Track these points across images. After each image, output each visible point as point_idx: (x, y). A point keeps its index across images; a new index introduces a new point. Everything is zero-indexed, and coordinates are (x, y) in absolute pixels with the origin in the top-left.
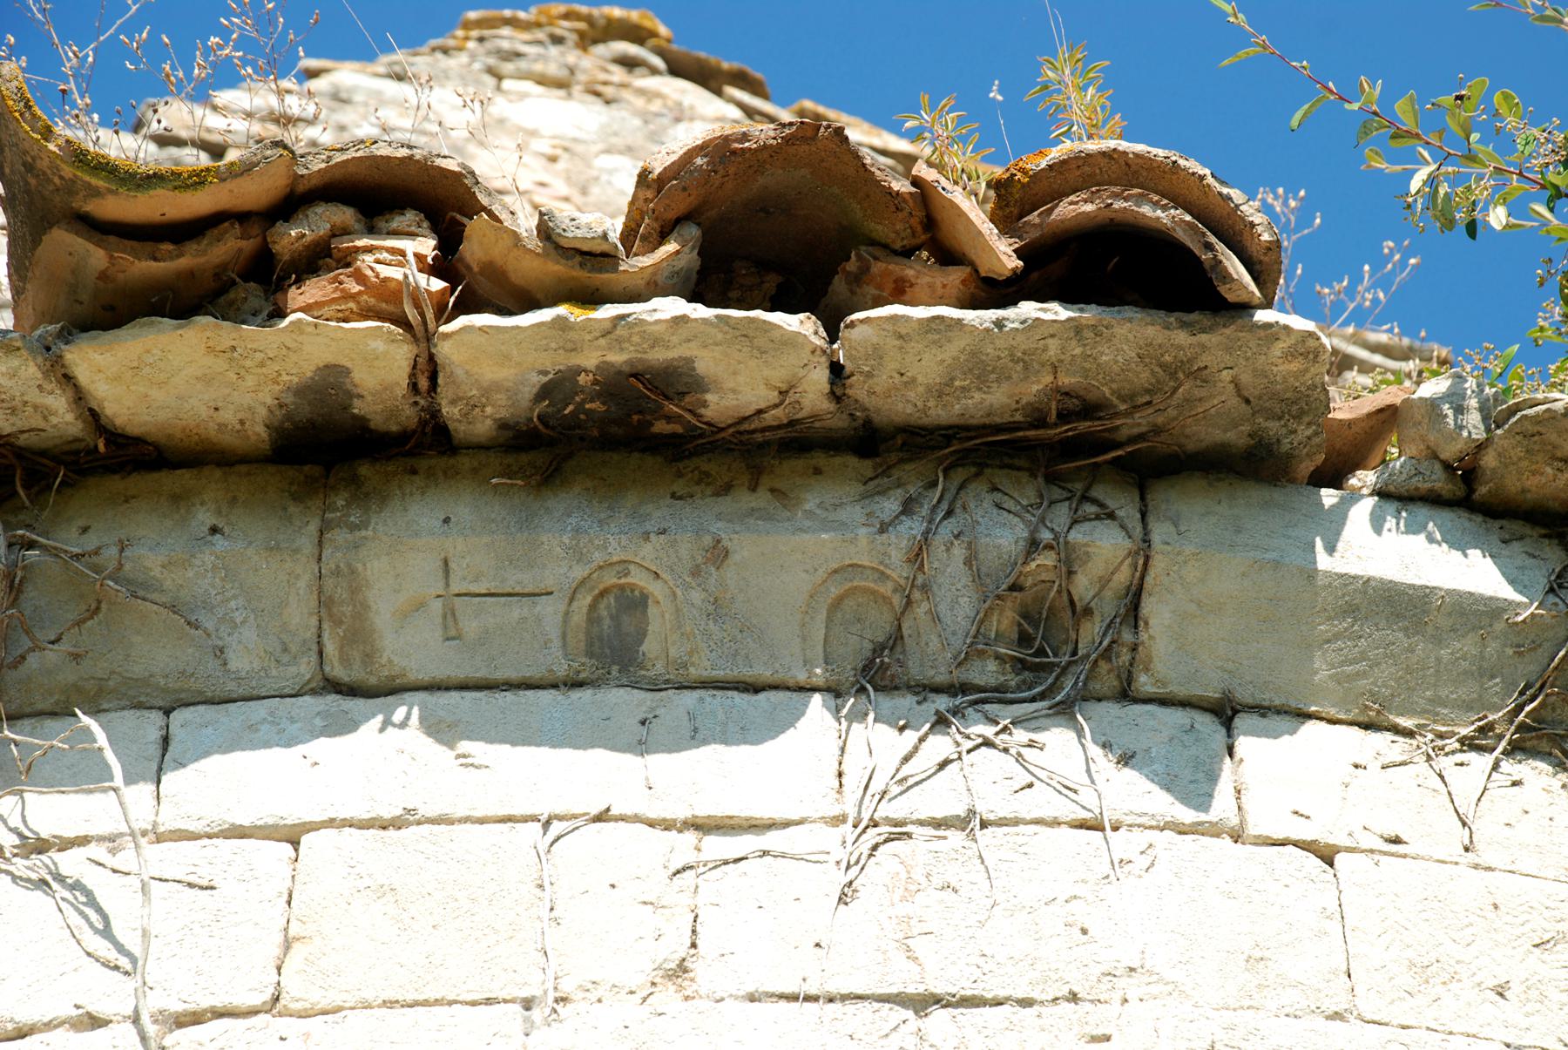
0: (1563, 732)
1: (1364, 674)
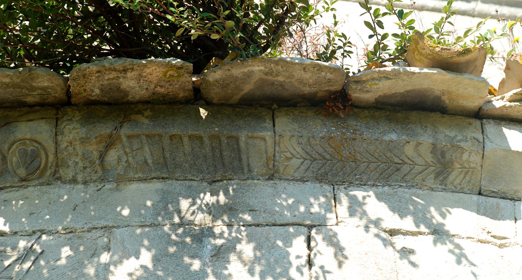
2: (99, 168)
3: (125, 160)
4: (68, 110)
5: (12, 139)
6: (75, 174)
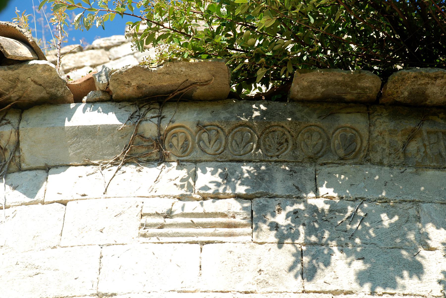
0: (137, 156)
1: (83, 152)
2: (402, 156)
3: (423, 151)
4: (377, 107)
5: (336, 125)
6: (382, 158)
